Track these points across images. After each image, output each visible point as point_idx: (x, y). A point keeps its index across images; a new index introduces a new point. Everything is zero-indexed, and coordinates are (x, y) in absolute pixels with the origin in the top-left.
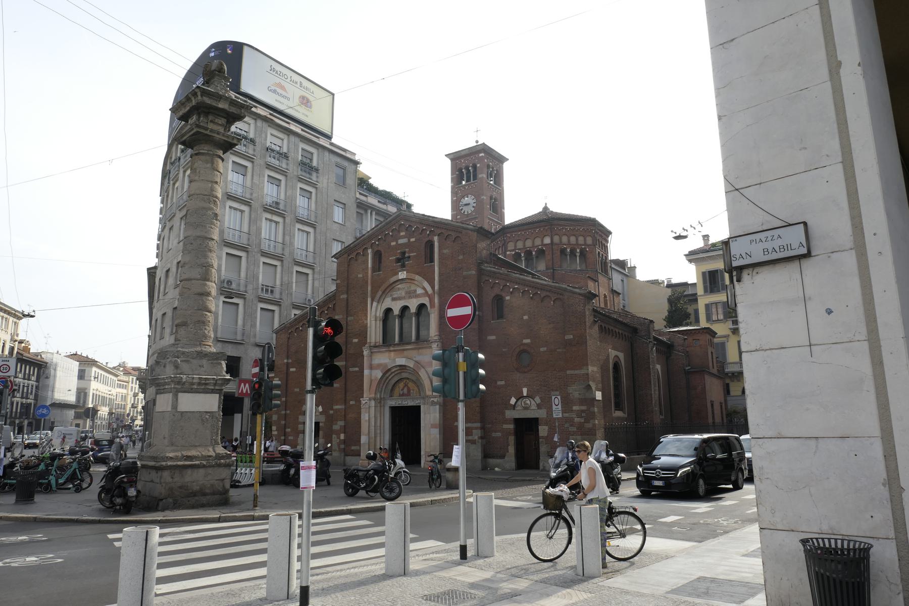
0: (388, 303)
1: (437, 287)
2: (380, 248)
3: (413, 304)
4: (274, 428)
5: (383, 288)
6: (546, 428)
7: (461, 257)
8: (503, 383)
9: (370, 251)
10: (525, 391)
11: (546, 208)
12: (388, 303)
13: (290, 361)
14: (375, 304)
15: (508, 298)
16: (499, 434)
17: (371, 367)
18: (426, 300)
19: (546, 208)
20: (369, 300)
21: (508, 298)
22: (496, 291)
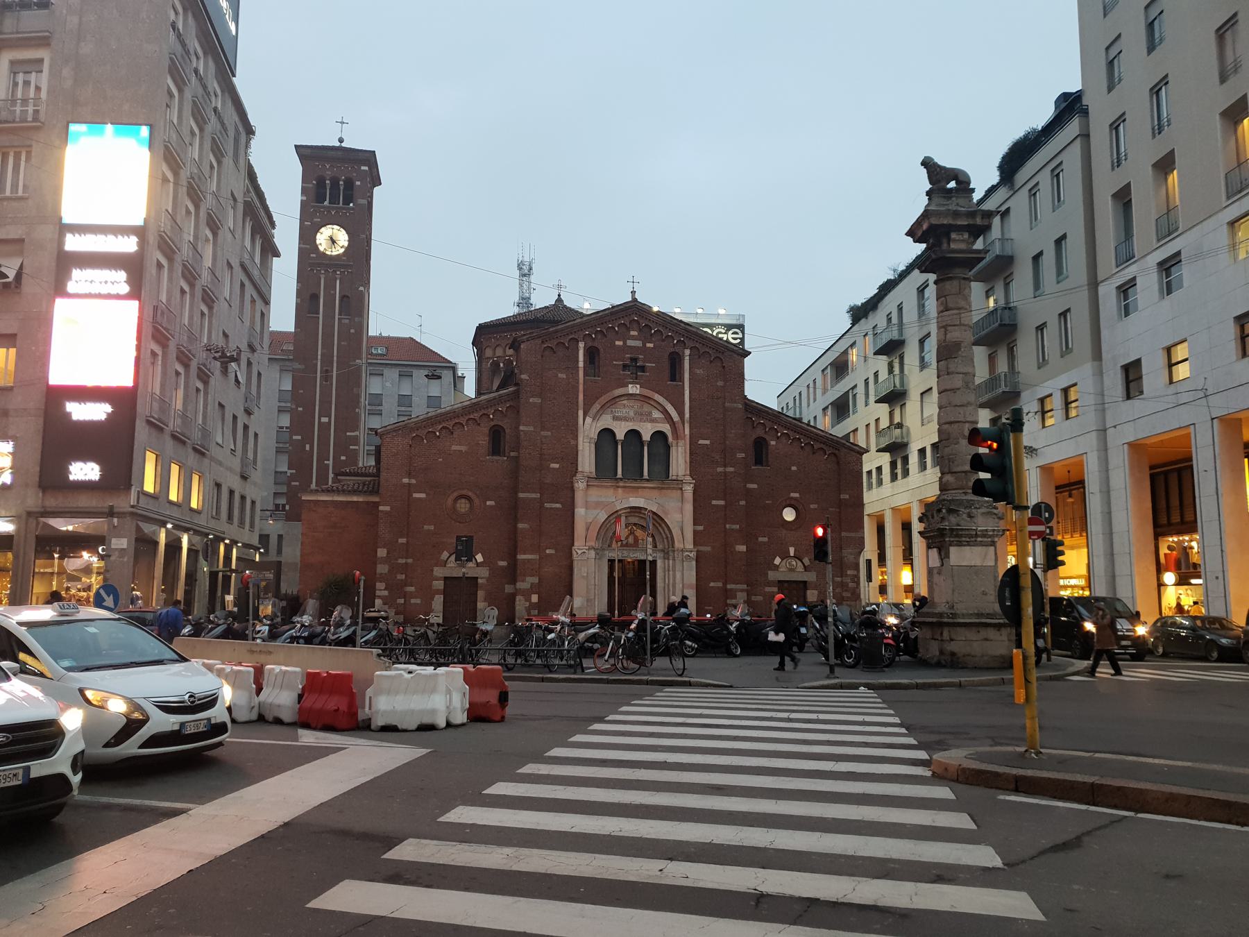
0: (606, 421)
1: (687, 415)
2: (596, 344)
3: (647, 432)
4: (380, 585)
5: (603, 399)
6: (816, 592)
7: (720, 383)
8: (765, 539)
9: (581, 345)
10: (792, 551)
11: (559, 300)
12: (606, 421)
13: (414, 481)
14: (589, 420)
15: (773, 443)
16: (760, 598)
17: (587, 506)
18: (666, 428)
19: (559, 300)
20: (581, 413)
21: (773, 443)
22: (759, 432)
